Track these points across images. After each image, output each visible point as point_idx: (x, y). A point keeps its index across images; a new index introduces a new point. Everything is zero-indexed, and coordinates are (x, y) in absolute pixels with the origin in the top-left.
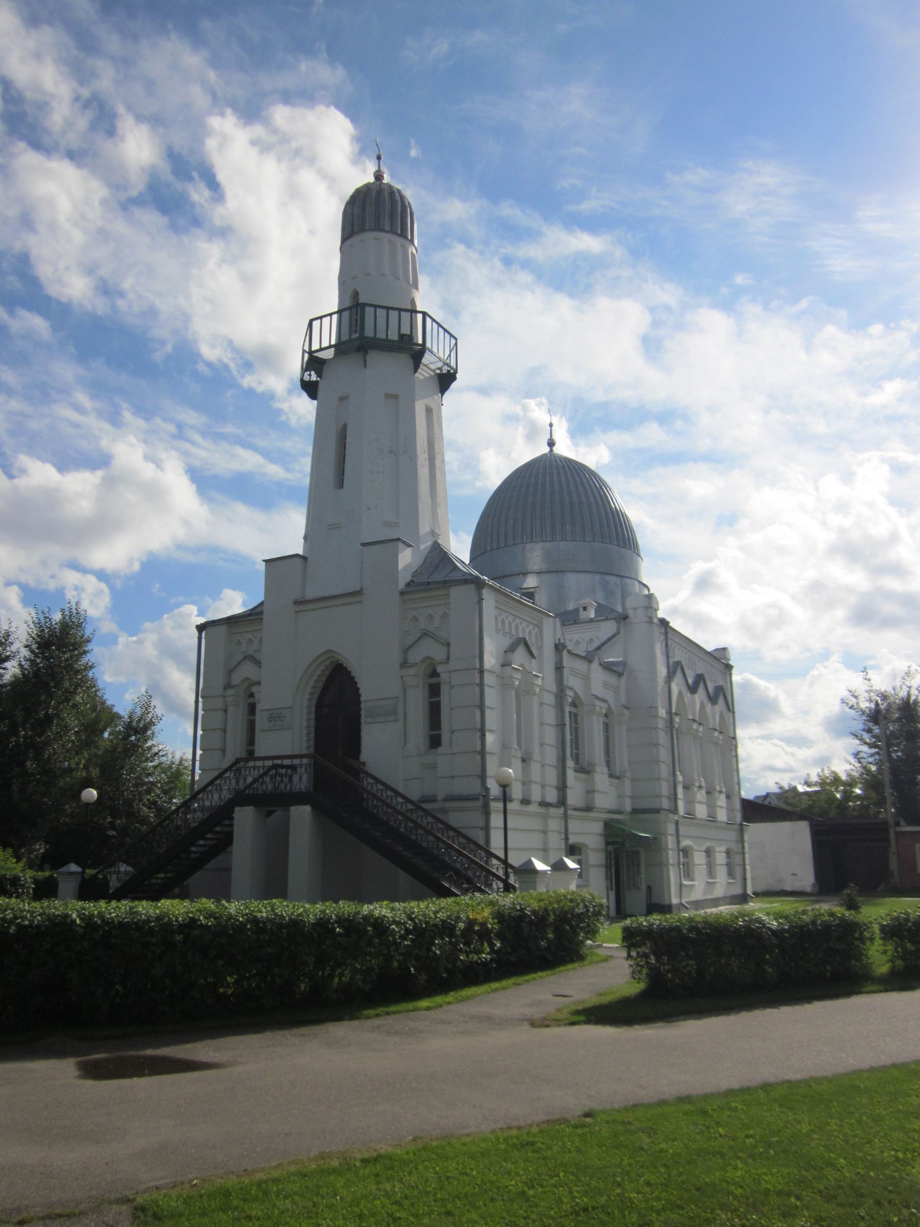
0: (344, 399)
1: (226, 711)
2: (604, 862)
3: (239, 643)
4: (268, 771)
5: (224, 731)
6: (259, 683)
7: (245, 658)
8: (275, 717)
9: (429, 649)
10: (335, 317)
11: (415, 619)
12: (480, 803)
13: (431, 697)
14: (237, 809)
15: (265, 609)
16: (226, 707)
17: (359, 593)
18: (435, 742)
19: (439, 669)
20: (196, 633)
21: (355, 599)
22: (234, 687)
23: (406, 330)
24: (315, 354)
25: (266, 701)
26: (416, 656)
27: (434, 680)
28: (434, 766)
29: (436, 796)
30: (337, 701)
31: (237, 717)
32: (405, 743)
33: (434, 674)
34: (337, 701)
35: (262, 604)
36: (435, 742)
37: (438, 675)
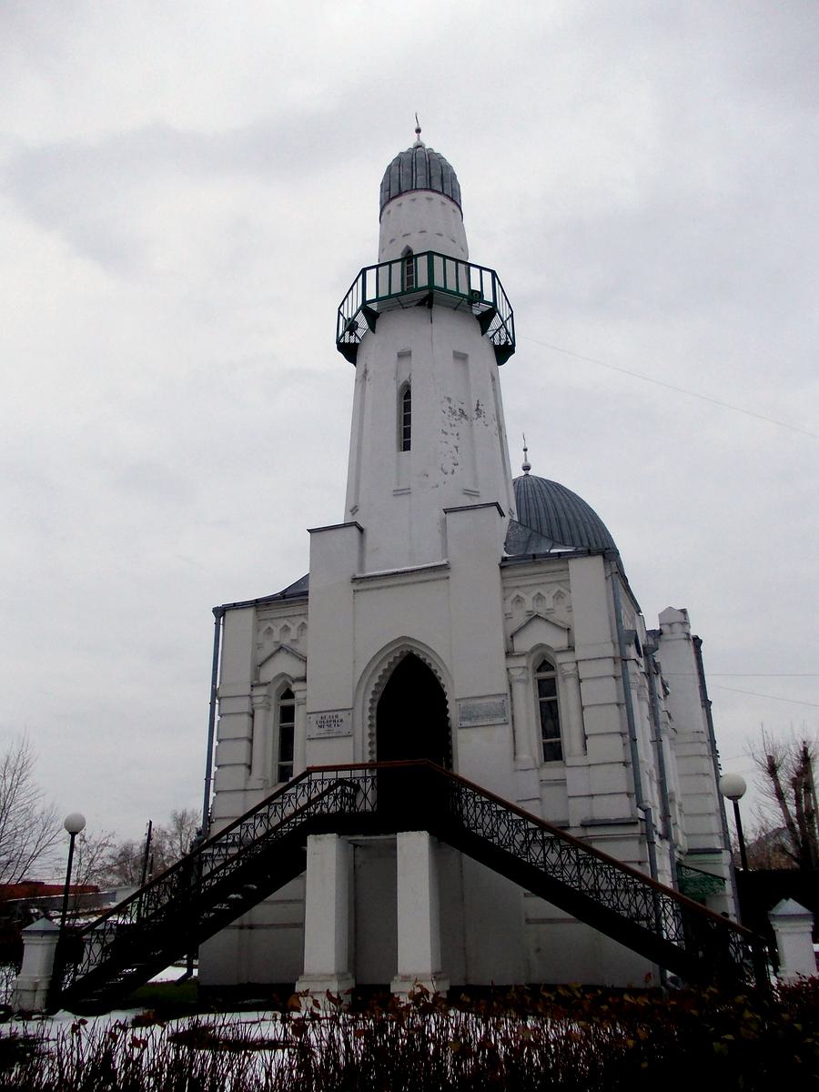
0: (404, 355)
1: (252, 716)
2: (472, 982)
3: (270, 631)
4: (331, 788)
5: (251, 741)
6: (304, 680)
7: (281, 648)
8: (329, 722)
9: (540, 635)
10: (397, 267)
11: (519, 600)
12: (637, 830)
13: (282, 721)
14: (311, 839)
15: (312, 588)
16: (254, 712)
17: (445, 567)
18: (553, 752)
19: (294, 688)
20: (213, 619)
21: (442, 574)
22: (265, 684)
23: (475, 286)
24: (369, 305)
25: (311, 700)
26: (524, 643)
27: (287, 702)
28: (562, 782)
29: (567, 822)
30: (411, 699)
31: (268, 725)
32: (515, 754)
33: (289, 694)
34: (411, 699)
35: (305, 579)
36: (553, 752)
37: (552, 668)
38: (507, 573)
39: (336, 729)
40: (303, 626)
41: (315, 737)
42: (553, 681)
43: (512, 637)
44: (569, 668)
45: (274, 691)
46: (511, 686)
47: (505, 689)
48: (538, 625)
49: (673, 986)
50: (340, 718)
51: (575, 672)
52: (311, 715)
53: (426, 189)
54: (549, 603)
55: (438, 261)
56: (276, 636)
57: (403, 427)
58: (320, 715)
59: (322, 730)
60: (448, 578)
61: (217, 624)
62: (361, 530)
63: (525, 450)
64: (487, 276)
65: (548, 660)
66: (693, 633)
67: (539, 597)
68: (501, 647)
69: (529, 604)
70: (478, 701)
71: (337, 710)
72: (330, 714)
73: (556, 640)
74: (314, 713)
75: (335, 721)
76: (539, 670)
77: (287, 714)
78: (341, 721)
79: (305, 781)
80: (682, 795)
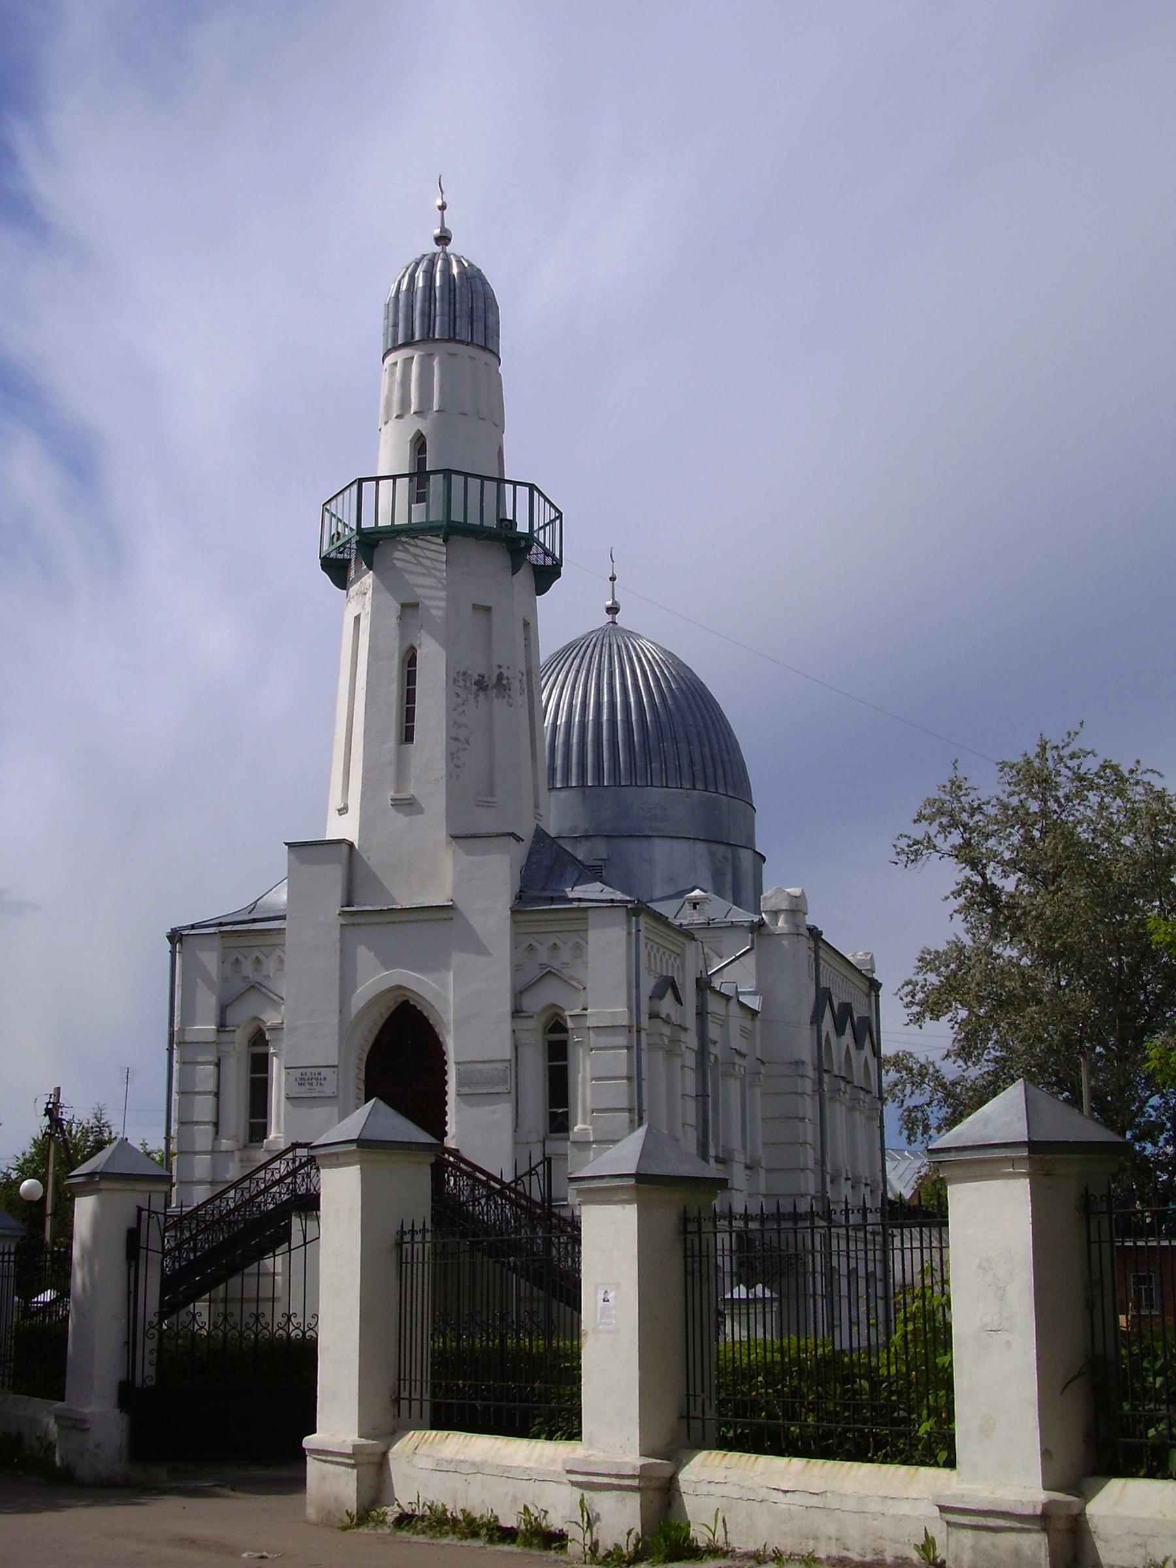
20: (169, 946)
27: (259, 1050)
38: (520, 917)
39: (319, 1088)
40: (281, 961)
46: (516, 1048)
47: (508, 1054)
49: (49, 1211)
50: (322, 1076)
53: (447, 341)
55: (457, 480)
57: (406, 687)
59: (303, 1089)
61: (173, 953)
63: (613, 579)
64: (523, 492)
66: (810, 920)
68: (507, 1008)
69: (543, 956)
70: (479, 1066)
77: (260, 1064)
79: (290, 1156)
80: (764, 1144)
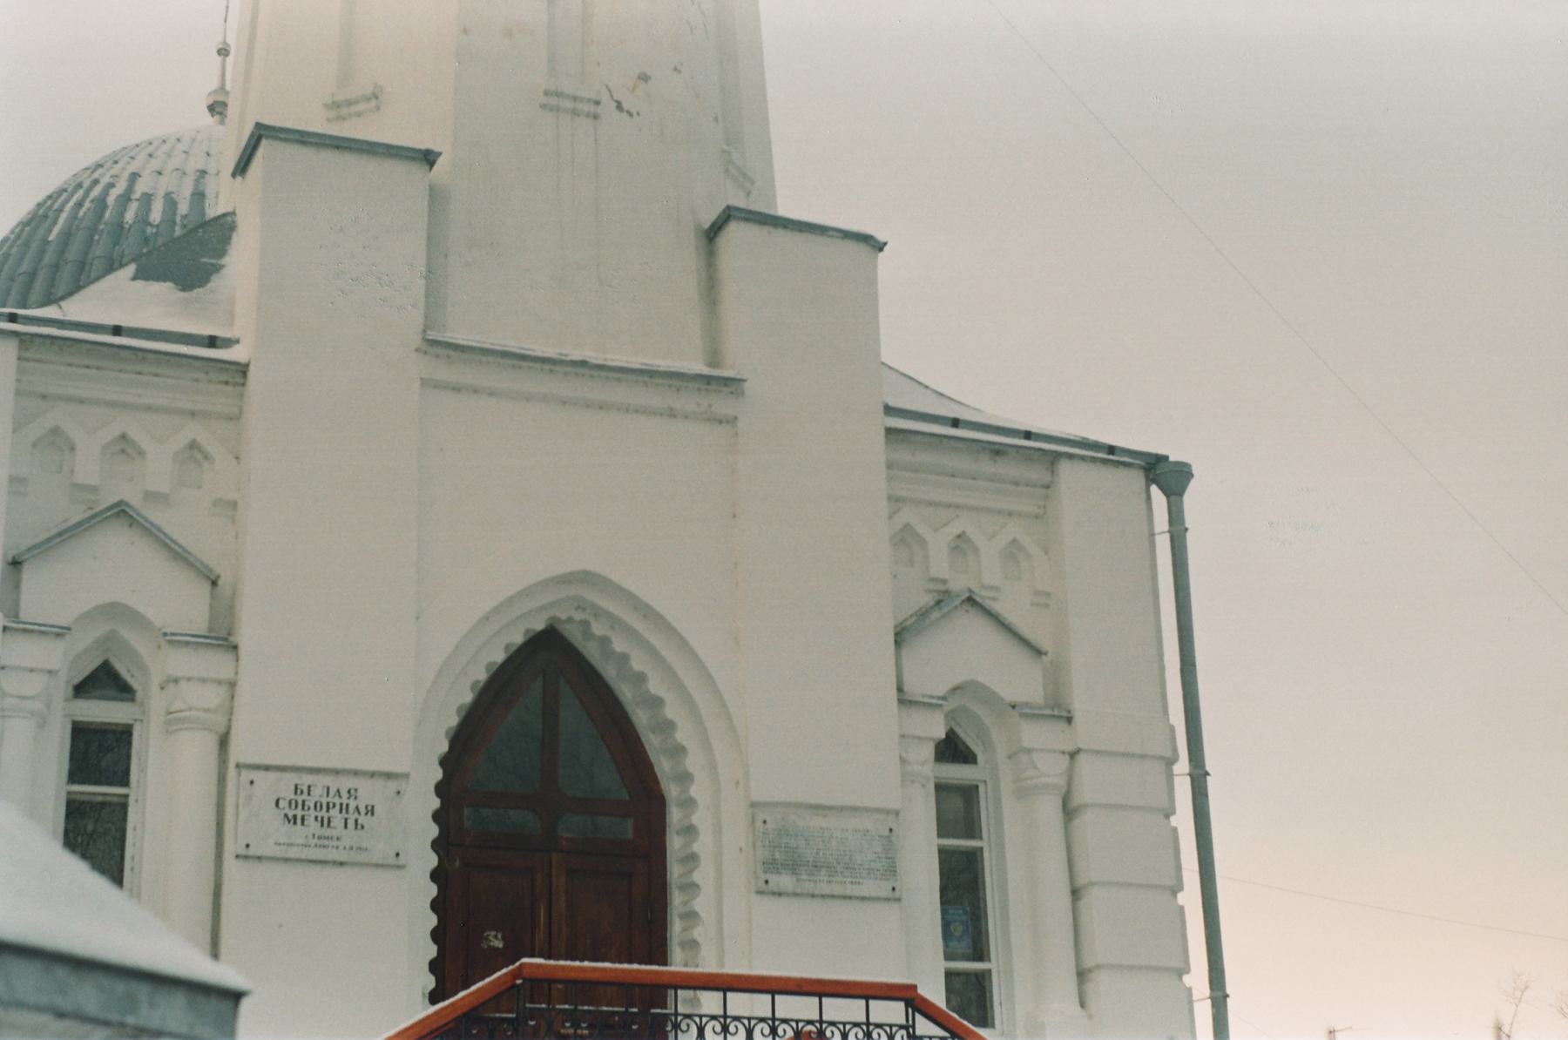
9: (962, 655)
39: (350, 837)
41: (270, 850)
42: (121, 736)
43: (16, 563)
44: (1051, 769)
45: (62, 660)
48: (116, 542)
51: (1062, 782)
52: (257, 776)
54: (158, 468)
56: (88, 466)
58: (291, 779)
60: (733, 421)
62: (728, 215)
65: (121, 668)
67: (961, 545)
70: (818, 822)
71: (356, 773)
72: (333, 782)
73: (174, 602)
74: (267, 768)
75: (344, 808)
76: (82, 689)
78: (371, 811)
